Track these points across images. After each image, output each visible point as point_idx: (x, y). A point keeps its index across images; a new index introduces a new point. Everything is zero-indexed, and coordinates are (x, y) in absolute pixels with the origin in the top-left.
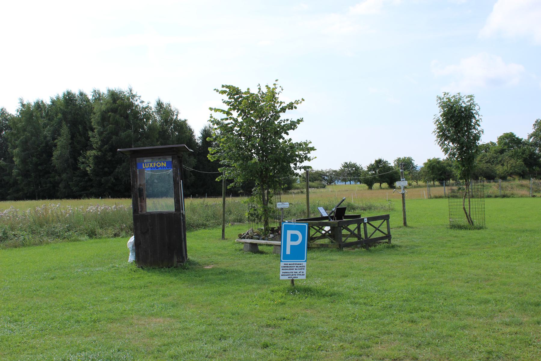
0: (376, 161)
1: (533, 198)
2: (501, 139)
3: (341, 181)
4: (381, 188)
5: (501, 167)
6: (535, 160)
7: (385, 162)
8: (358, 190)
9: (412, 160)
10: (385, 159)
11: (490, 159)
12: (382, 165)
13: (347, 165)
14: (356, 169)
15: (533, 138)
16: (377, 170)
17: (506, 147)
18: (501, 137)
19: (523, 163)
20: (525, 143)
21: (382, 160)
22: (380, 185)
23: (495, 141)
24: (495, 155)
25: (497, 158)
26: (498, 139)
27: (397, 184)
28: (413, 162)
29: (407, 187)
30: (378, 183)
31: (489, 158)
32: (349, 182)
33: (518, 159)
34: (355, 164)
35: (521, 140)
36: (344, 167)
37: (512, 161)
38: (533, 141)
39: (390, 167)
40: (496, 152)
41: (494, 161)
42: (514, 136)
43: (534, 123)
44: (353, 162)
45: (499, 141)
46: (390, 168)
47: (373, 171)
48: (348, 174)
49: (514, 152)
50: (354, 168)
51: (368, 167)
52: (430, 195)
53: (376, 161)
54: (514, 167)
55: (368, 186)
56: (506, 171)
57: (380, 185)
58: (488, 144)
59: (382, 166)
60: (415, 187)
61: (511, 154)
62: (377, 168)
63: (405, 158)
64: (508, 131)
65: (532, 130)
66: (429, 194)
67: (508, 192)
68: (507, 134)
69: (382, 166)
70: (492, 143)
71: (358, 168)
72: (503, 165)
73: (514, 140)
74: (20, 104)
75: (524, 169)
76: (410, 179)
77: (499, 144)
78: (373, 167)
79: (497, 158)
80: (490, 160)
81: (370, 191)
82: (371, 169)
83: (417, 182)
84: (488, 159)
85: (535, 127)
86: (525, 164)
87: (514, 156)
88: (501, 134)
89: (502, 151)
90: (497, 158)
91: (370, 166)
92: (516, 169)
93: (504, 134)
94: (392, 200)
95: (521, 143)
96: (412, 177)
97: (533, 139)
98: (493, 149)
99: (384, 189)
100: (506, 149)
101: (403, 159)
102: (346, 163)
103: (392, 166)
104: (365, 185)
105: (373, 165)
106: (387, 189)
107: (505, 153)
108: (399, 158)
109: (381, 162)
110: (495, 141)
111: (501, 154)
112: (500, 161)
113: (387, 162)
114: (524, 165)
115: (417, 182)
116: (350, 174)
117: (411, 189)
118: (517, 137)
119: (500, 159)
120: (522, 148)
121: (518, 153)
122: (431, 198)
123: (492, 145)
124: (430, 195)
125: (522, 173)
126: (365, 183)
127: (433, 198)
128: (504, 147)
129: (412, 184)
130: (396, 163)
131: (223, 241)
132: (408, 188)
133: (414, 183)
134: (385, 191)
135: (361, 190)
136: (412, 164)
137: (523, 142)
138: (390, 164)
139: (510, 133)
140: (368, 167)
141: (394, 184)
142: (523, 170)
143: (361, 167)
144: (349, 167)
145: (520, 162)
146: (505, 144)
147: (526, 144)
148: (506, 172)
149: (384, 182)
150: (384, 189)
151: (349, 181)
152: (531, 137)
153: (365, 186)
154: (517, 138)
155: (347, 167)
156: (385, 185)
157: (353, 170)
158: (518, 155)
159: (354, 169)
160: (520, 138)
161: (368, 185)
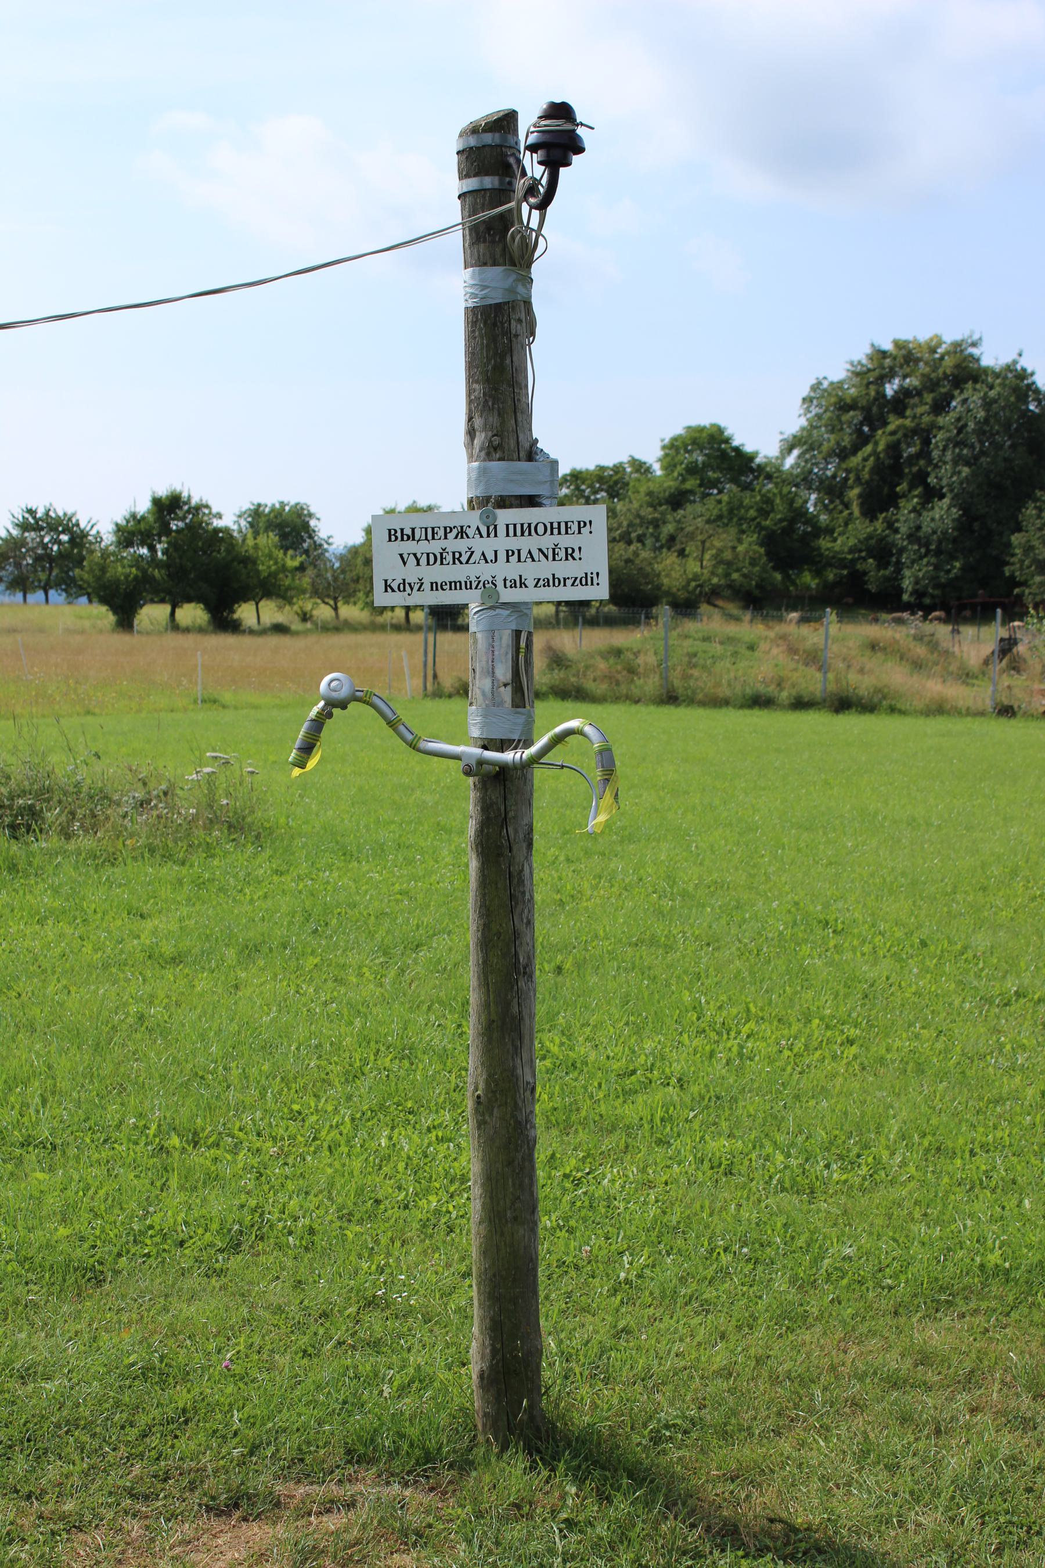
0: (157, 502)
1: (1003, 720)
2: (674, 448)
3: (7, 588)
4: (174, 625)
5: (678, 561)
6: (807, 539)
7: (198, 508)
8: (68, 631)
9: (310, 515)
10: (196, 492)
11: (629, 525)
12: (183, 519)
13: (34, 518)
14: (72, 541)
15: (796, 452)
16: (160, 542)
17: (691, 483)
18: (675, 439)
19: (762, 550)
20: (766, 472)
21: (185, 494)
22: (173, 614)
23: (652, 455)
24: (648, 513)
25: (657, 527)
26: (664, 448)
27: (245, 613)
28: (313, 523)
29: (293, 627)
30: (162, 601)
31: (625, 523)
32: (40, 594)
33: (743, 532)
34: (70, 519)
35: (750, 458)
36: (24, 526)
37: (722, 540)
38: (797, 465)
39: (217, 531)
40: (654, 501)
41: (644, 535)
42: (727, 441)
43: (805, 391)
44: (61, 508)
45: (666, 455)
46: (219, 538)
47: (142, 544)
48: (38, 559)
49: (728, 503)
50: (63, 532)
51: (117, 525)
52: (435, 676)
53: (157, 502)
54: (729, 564)
55: (115, 612)
56: (696, 577)
57: (173, 614)
58: (618, 469)
59: (181, 524)
60: (326, 628)
61: (715, 512)
62: (160, 535)
63: (283, 504)
64: (704, 419)
65: (795, 422)
66: (430, 673)
67: (861, 684)
68: (701, 430)
69: (181, 524)
70: (640, 467)
71: (84, 535)
72: (682, 553)
73: (724, 454)
74: (52, 593)
75: (764, 575)
76: (304, 592)
77: (664, 468)
78: (142, 526)
79: (656, 524)
80: (629, 533)
81: (123, 639)
82: (132, 533)
83: (336, 609)
84: (620, 525)
85: (808, 410)
86: (768, 553)
87: (731, 516)
88: (675, 428)
89: (677, 500)
90: (656, 524)
91: (128, 521)
92: (735, 576)
93: (689, 428)
94: (227, 697)
95: (752, 470)
96: (313, 584)
97: (799, 457)
98: (643, 489)
99: (187, 630)
100: (691, 492)
101: (273, 509)
102: (31, 512)
103: (227, 530)
104: (103, 609)
105: (143, 518)
106: (201, 630)
107: (689, 508)
108: (259, 505)
109: (181, 508)
110: (652, 455)
111: (674, 510)
112: (672, 539)
113: (207, 506)
114: (764, 559)
115: (336, 609)
116: (44, 559)
117: (311, 639)
118: (736, 443)
119: (669, 529)
120: (760, 491)
121: (743, 511)
122: (438, 694)
123: (637, 471)
124: (435, 676)
125: (757, 593)
126: (103, 601)
127: (450, 696)
128: (684, 481)
129: (315, 613)
130: (243, 523)
131: (228, 640)
132: (296, 633)
133: (323, 612)
134: (188, 641)
135: (83, 632)
136: (311, 533)
137: (759, 466)
138: (219, 516)
139: (713, 425)
140: (117, 525)
141: (233, 612)
142: (762, 580)
143: (93, 532)
144: (42, 529)
145: (749, 545)
146: (692, 470)
147: (769, 477)
148: (693, 584)
149: (189, 600)
150: (187, 630)
151: (40, 587)
152: (790, 450)
153: (103, 615)
154: (737, 450)
155: (34, 530)
156: (192, 613)
157: (60, 543)
158: (740, 519)
159: (65, 538)
160: (748, 448)
161: (115, 609)
